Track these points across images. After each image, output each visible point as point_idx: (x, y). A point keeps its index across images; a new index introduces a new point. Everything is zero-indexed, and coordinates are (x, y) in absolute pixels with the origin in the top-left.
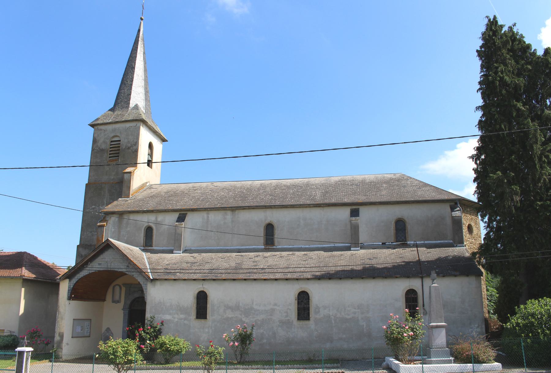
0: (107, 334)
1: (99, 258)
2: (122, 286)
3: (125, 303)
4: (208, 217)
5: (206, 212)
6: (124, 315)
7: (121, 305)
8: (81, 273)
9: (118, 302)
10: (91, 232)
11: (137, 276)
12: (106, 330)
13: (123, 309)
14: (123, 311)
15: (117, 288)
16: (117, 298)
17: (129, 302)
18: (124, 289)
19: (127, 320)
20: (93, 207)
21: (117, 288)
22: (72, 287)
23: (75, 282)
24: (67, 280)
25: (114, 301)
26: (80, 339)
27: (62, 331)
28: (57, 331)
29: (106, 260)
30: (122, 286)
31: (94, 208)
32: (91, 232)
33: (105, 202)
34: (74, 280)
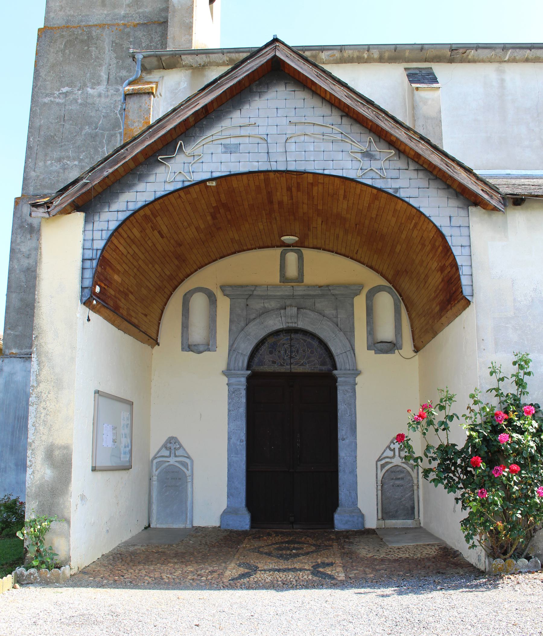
0: (172, 460)
1: (226, 123)
2: (219, 295)
3: (232, 349)
4: (502, 81)
5: (495, 65)
6: (232, 393)
7: (219, 357)
8: (141, 186)
9: (209, 346)
10: (59, 160)
11: (414, 192)
12: (165, 446)
13: (228, 373)
14: (225, 380)
15: (199, 302)
16: (198, 334)
17: (246, 347)
18: (224, 305)
19: (242, 410)
20: (64, 90)
21: (199, 302)
22: (100, 245)
23: (113, 225)
24: (80, 216)
25: (188, 347)
26: (117, 473)
27: (60, 441)
28: (38, 439)
29: (262, 131)
30: (219, 295)
31: (66, 94)
32: (59, 160)
33: (104, 77)
34: (111, 216)
